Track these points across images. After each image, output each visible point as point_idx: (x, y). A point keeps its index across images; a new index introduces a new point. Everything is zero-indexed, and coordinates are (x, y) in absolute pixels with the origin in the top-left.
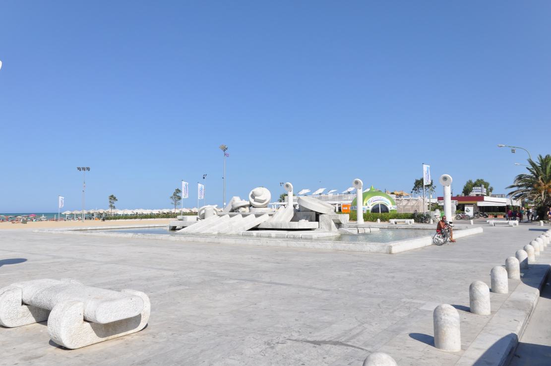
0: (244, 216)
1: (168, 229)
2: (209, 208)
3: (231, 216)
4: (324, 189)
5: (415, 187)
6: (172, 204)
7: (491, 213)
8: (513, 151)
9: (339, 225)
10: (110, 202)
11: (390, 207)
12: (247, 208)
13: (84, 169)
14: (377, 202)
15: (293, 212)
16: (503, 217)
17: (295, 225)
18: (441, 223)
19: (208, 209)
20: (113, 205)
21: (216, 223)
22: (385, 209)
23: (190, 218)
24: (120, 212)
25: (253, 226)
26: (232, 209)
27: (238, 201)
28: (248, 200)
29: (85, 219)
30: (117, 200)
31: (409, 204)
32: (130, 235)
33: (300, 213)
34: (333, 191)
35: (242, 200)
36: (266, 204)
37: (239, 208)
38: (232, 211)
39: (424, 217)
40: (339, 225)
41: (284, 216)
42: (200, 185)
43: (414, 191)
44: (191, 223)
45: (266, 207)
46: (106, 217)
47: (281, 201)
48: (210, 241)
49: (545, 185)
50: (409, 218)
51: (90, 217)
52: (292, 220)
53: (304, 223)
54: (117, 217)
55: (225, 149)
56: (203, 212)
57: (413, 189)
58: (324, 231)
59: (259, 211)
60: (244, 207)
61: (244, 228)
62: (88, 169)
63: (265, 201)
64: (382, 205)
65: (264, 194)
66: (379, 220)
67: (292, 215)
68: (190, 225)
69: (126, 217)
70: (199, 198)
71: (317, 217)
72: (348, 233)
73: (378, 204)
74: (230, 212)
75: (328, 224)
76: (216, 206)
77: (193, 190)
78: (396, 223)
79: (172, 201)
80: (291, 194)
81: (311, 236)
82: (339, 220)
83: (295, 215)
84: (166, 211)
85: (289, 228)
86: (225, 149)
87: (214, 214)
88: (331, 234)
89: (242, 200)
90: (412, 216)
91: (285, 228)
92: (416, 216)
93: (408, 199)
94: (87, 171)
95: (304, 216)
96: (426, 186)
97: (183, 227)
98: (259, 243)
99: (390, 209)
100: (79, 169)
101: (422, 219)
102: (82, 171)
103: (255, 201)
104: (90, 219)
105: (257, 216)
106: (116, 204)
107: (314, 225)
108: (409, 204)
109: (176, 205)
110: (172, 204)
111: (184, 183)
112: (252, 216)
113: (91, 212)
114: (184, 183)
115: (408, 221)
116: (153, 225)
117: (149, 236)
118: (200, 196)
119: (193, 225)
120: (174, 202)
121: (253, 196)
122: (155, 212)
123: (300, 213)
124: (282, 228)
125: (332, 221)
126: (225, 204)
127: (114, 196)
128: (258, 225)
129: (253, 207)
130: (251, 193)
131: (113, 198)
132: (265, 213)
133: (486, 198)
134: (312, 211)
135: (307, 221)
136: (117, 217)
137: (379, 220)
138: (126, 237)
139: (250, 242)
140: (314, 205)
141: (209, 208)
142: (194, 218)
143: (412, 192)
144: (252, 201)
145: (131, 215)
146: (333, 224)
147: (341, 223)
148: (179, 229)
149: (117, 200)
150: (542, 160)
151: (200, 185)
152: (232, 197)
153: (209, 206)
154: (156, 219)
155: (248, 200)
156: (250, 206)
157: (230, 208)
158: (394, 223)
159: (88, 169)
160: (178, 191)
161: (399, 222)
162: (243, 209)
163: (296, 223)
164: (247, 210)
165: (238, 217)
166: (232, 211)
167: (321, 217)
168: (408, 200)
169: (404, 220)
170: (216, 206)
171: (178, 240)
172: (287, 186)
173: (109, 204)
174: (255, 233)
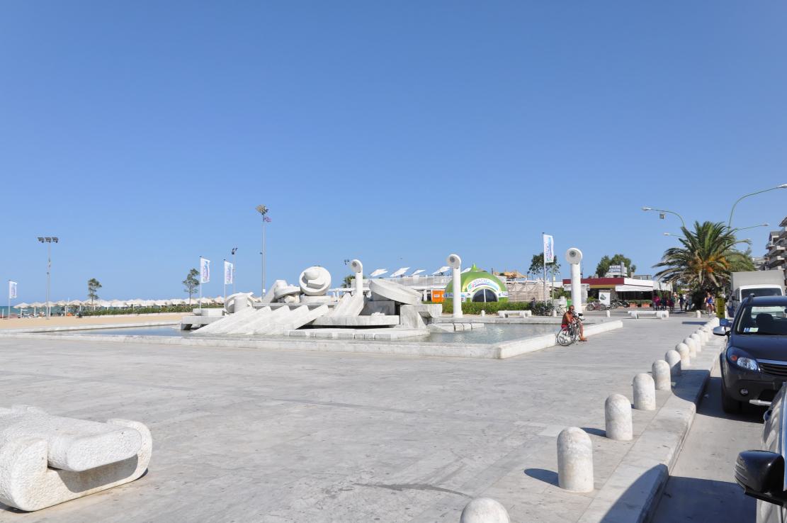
0: (292, 308)
1: (180, 328)
2: (241, 297)
3: (273, 308)
4: (407, 269)
5: (532, 266)
6: (185, 291)
7: (633, 301)
8: (662, 217)
9: (428, 319)
10: (90, 289)
11: (499, 293)
12: (297, 297)
13: (48, 240)
14: (482, 287)
15: (363, 302)
16: (648, 306)
17: (366, 320)
18: (567, 315)
19: (240, 298)
20: (95, 293)
21: (251, 319)
22: (491, 297)
23: (212, 312)
24: (106, 305)
25: (306, 322)
26: (275, 298)
27: (283, 287)
28: (298, 285)
29: (51, 314)
30: (100, 286)
31: (524, 290)
32: (122, 338)
33: (373, 303)
34: (419, 271)
35: (289, 285)
36: (325, 290)
37: (284, 296)
38: (275, 301)
39: (545, 307)
40: (428, 319)
41: (350, 307)
42: (227, 264)
43: (531, 271)
44: (213, 320)
45: (325, 295)
46: (85, 312)
47: (345, 287)
48: (242, 345)
49: (702, 263)
50: (525, 309)
51: (59, 311)
52: (362, 314)
53: (378, 318)
54: (101, 312)
55: (264, 212)
56: (232, 302)
57: (530, 269)
58: (407, 329)
59: (313, 300)
60: (292, 295)
61: (292, 326)
62: (56, 240)
63: (322, 286)
64: (490, 292)
65: (321, 276)
66: (483, 312)
67: (361, 307)
68: (213, 322)
69: (115, 311)
70: (226, 283)
71: (397, 308)
72: (441, 332)
73: (482, 291)
74: (272, 302)
75: (412, 318)
76: (251, 293)
77: (216, 270)
78: (507, 316)
79: (185, 287)
80: (359, 276)
81: (390, 335)
82: (428, 313)
83: (366, 305)
84: (177, 302)
85: (357, 324)
86: (264, 212)
87: (249, 306)
88: (417, 333)
89: (289, 285)
90: (529, 307)
91: (352, 325)
92: (534, 306)
93: (522, 282)
94: (53, 243)
95: (379, 307)
96: (547, 264)
97: (203, 325)
98: (314, 347)
99: (498, 297)
100: (41, 240)
101: (542, 309)
102: (46, 243)
103: (307, 286)
104: (59, 314)
105: (311, 308)
106: (99, 292)
107: (393, 319)
108: (524, 290)
109: (191, 293)
110: (185, 291)
111: (203, 261)
112: (304, 308)
113: (61, 304)
114: (203, 261)
115: (523, 313)
116: (156, 323)
117: (150, 339)
118: (227, 281)
119: (217, 323)
120: (188, 289)
121: (305, 280)
122: (160, 303)
123: (373, 303)
124: (348, 325)
125: (418, 314)
126: (264, 291)
127: (97, 280)
128: (313, 321)
129: (306, 295)
130: (302, 275)
131: (94, 283)
132: (323, 304)
133: (627, 281)
134: (390, 300)
135: (384, 314)
136: (101, 312)
137: (483, 312)
138: (115, 340)
139: (302, 345)
140: (393, 292)
141: (241, 296)
142: (218, 311)
143: (528, 272)
144: (304, 286)
145: (123, 308)
146: (419, 318)
147: (431, 317)
148: (196, 329)
149: (100, 286)
150: (698, 229)
151: (227, 264)
152: (275, 281)
153: (241, 294)
154: (161, 314)
155: (298, 285)
156: (301, 293)
157: (272, 297)
158: (504, 316)
159: (56, 240)
160: (195, 272)
161: (511, 314)
162: (291, 298)
163: (367, 317)
164: (296, 299)
165: (284, 310)
166: (275, 301)
167: (402, 309)
168: (524, 284)
169: (517, 312)
170: (251, 293)
171: (194, 343)
172: (355, 264)
173: (89, 293)
174: (308, 332)
